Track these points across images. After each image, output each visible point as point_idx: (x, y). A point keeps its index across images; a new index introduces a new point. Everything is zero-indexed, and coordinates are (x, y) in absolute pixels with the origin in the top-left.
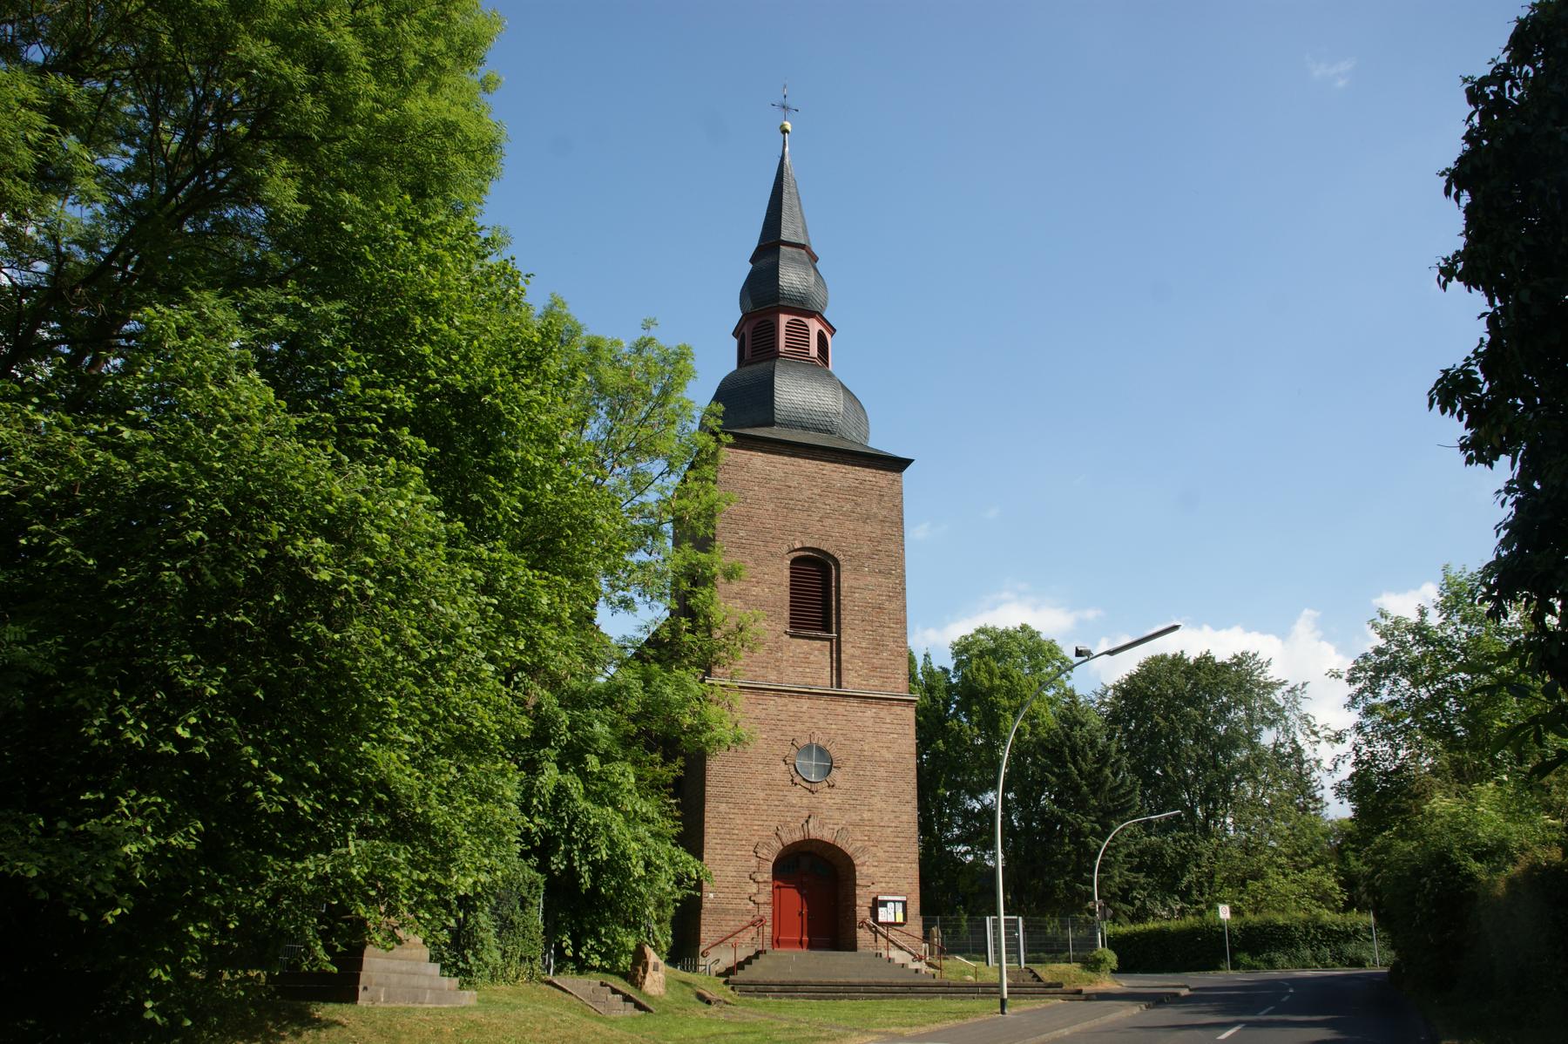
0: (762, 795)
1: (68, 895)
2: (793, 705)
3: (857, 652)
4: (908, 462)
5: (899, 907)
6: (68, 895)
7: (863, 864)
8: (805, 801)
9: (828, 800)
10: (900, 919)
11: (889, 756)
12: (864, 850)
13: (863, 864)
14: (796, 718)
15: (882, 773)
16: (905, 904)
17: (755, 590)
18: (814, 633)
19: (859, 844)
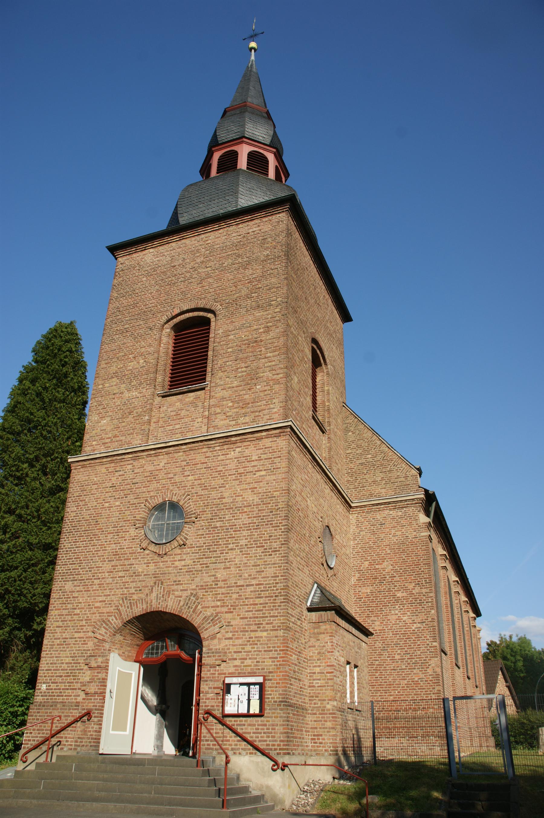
0: (107, 566)
1: (26, 591)
2: (146, 465)
3: (226, 394)
4: (372, 634)
5: (255, 690)
6: (26, 591)
7: (213, 637)
8: (152, 567)
9: (180, 560)
10: (255, 709)
11: (251, 497)
12: (214, 619)
13: (213, 637)
14: (153, 476)
15: (244, 519)
16: (261, 686)
17: (131, 365)
18: (184, 389)
19: (209, 612)
